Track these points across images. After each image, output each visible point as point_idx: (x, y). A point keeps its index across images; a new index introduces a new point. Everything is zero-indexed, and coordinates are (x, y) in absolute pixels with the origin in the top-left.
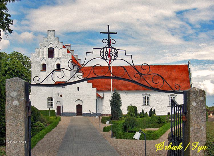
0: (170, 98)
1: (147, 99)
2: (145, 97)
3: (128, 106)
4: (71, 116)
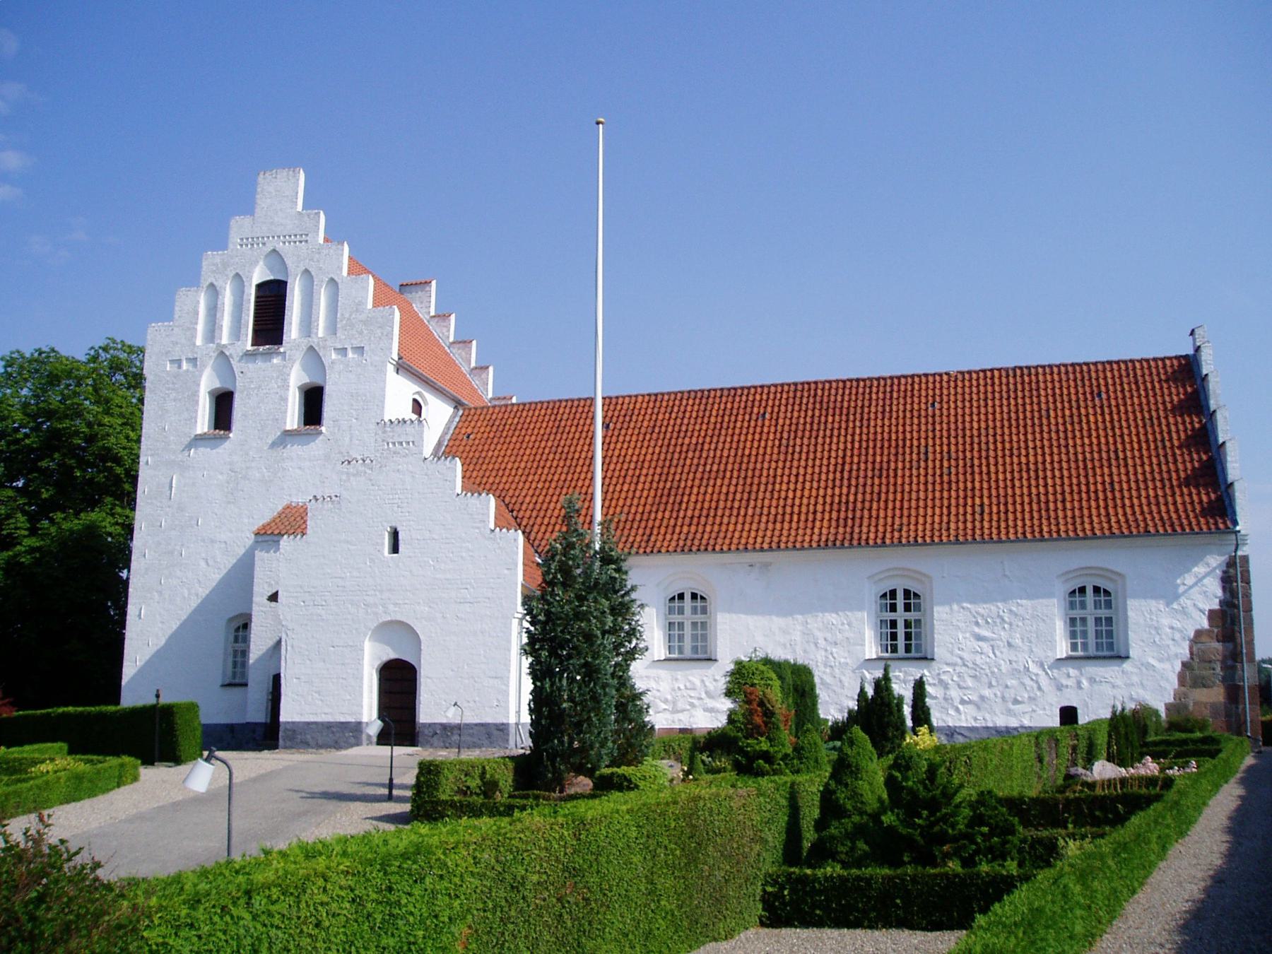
0: (884, 596)
1: (907, 608)
2: (893, 593)
3: (739, 663)
4: (337, 746)
